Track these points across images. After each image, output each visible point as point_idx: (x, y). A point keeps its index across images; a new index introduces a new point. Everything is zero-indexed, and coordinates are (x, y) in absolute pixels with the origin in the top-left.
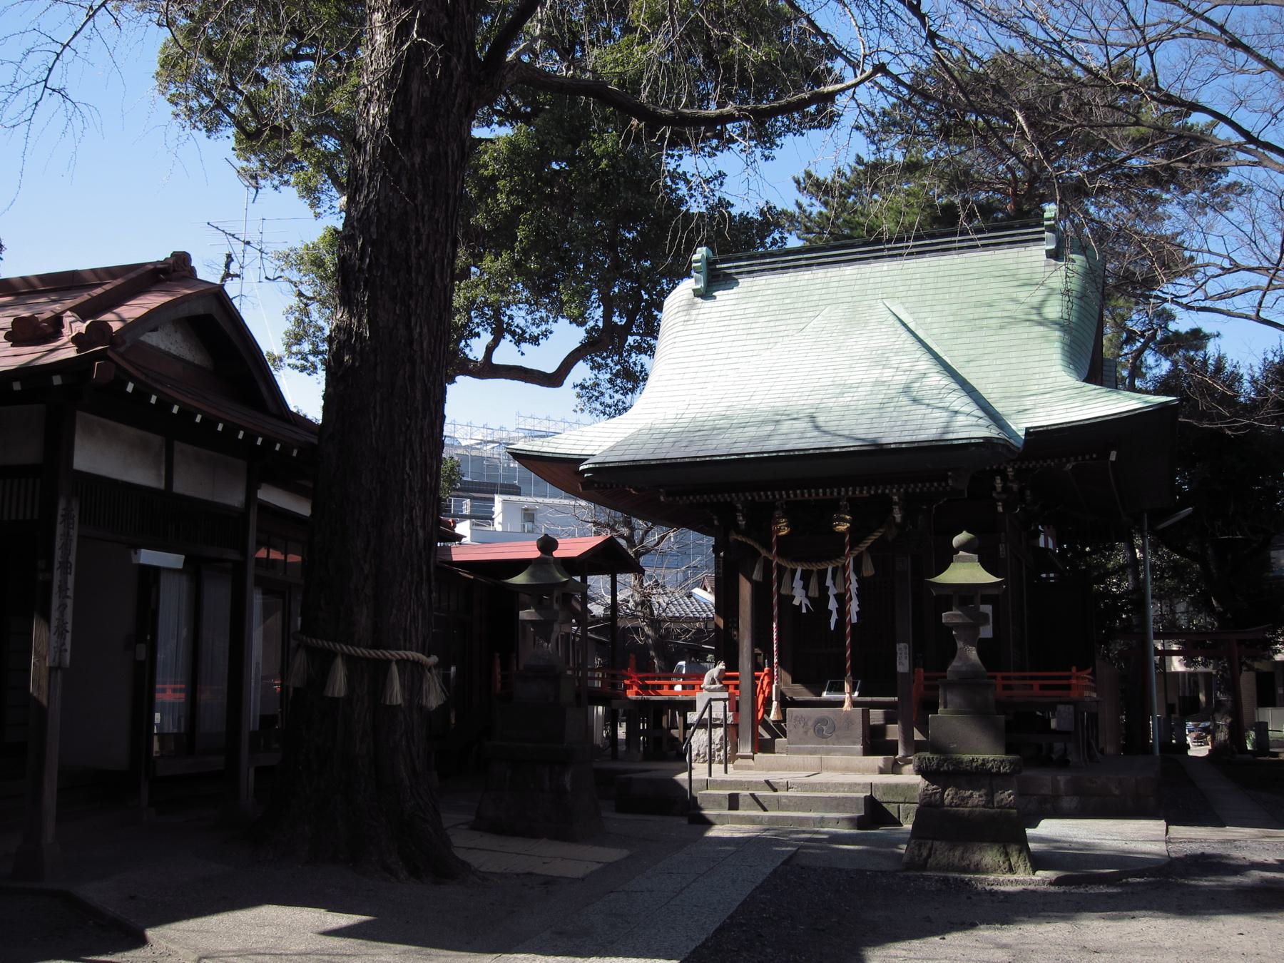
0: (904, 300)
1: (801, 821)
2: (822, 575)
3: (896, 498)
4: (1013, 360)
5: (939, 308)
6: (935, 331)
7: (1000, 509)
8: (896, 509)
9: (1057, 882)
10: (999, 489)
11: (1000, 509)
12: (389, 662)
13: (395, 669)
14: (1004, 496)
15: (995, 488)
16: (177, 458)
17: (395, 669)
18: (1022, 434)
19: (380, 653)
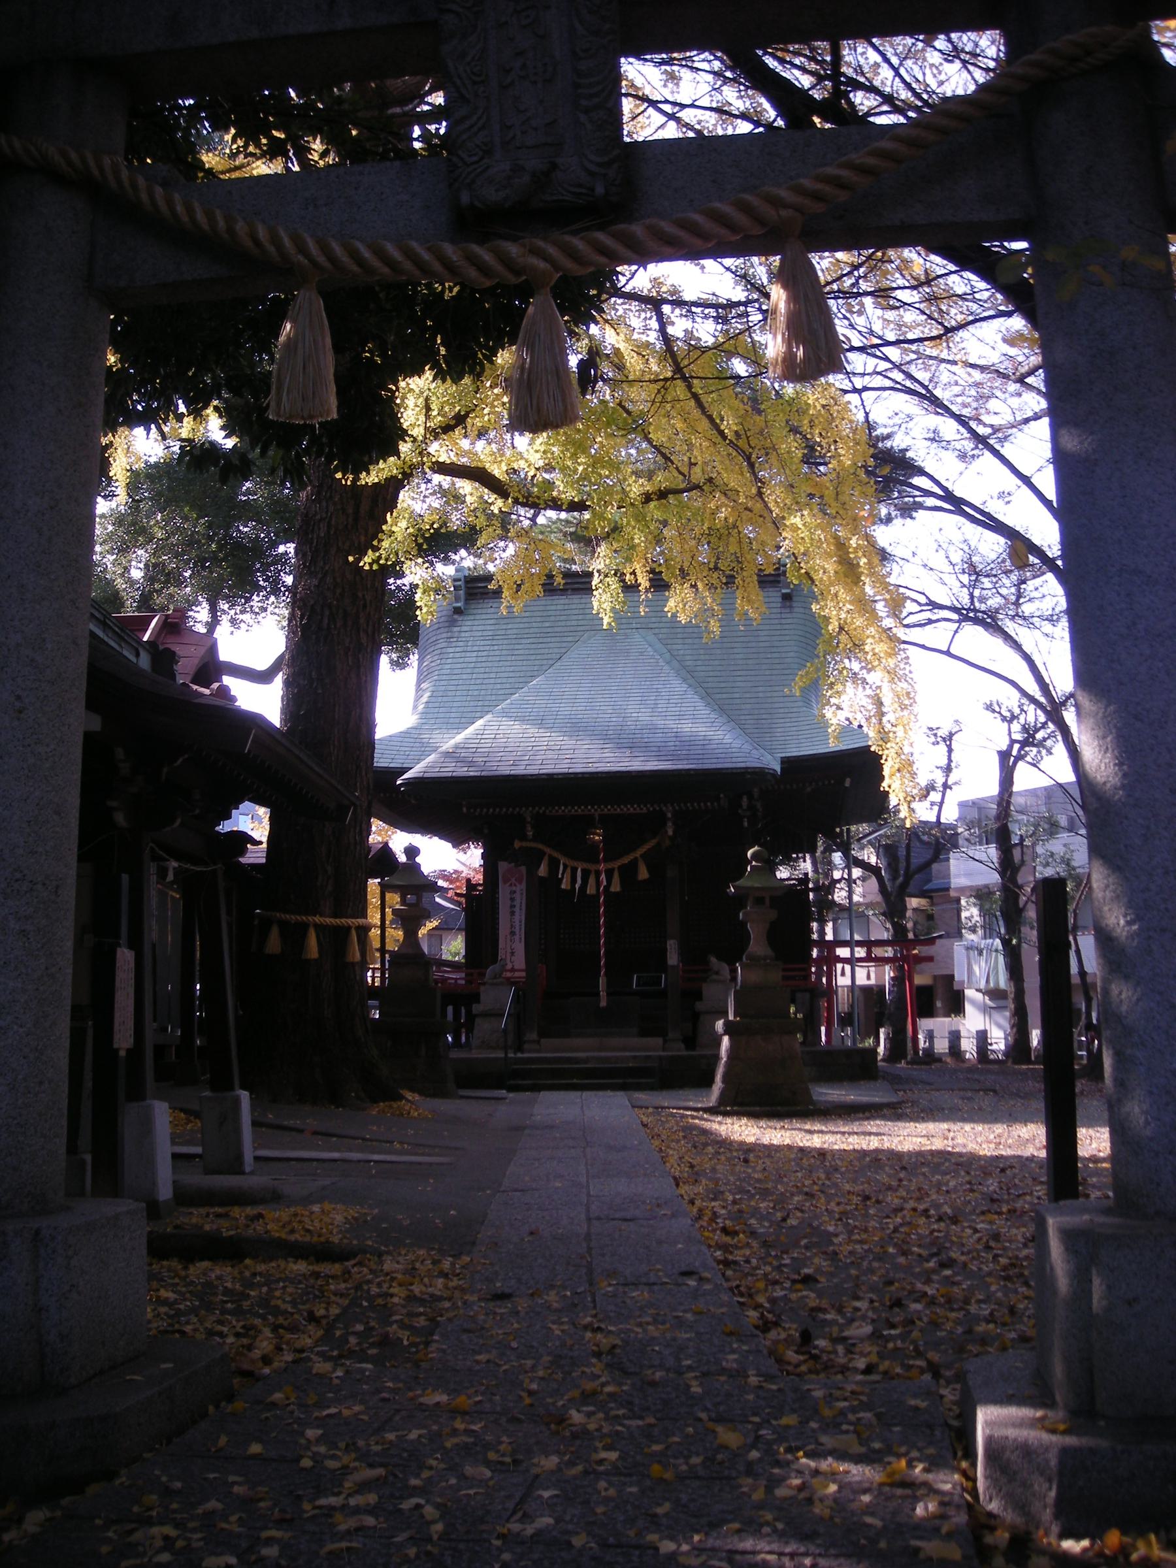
0: (657, 631)
1: (331, 1150)
2: (598, 874)
3: (669, 815)
4: (761, 695)
5: (690, 641)
6: (688, 663)
7: (746, 824)
8: (670, 824)
9: (393, 1537)
10: (745, 807)
11: (746, 824)
12: (349, 928)
13: (354, 933)
14: (748, 813)
15: (740, 806)
16: (855, 925)
17: (354, 933)
18: (778, 768)
19: (344, 921)
